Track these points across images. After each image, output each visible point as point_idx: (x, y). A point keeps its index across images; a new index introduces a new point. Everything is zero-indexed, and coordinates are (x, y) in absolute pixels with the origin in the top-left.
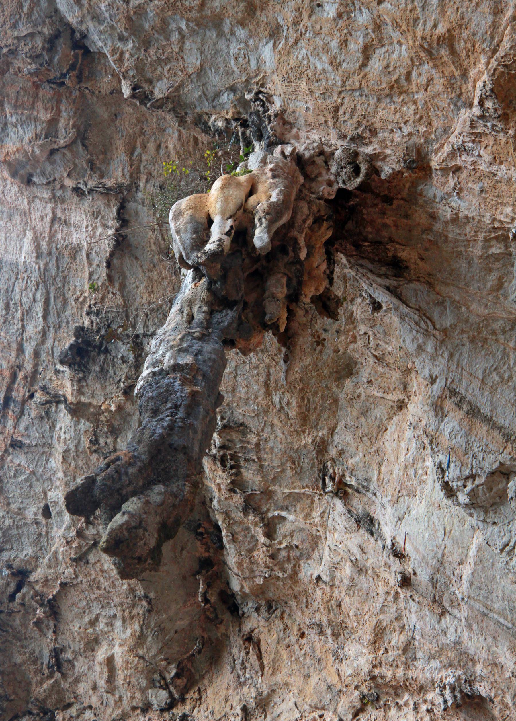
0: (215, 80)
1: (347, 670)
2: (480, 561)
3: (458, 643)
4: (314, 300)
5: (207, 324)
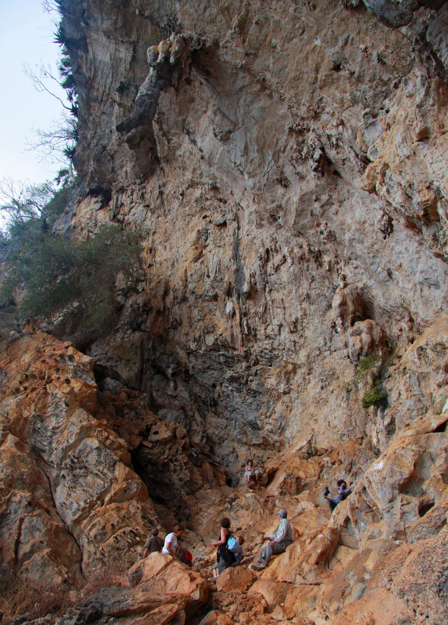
0: (163, 12)
1: (185, 178)
2: (221, 154)
3: (214, 174)
4: (185, 80)
5: (156, 83)
